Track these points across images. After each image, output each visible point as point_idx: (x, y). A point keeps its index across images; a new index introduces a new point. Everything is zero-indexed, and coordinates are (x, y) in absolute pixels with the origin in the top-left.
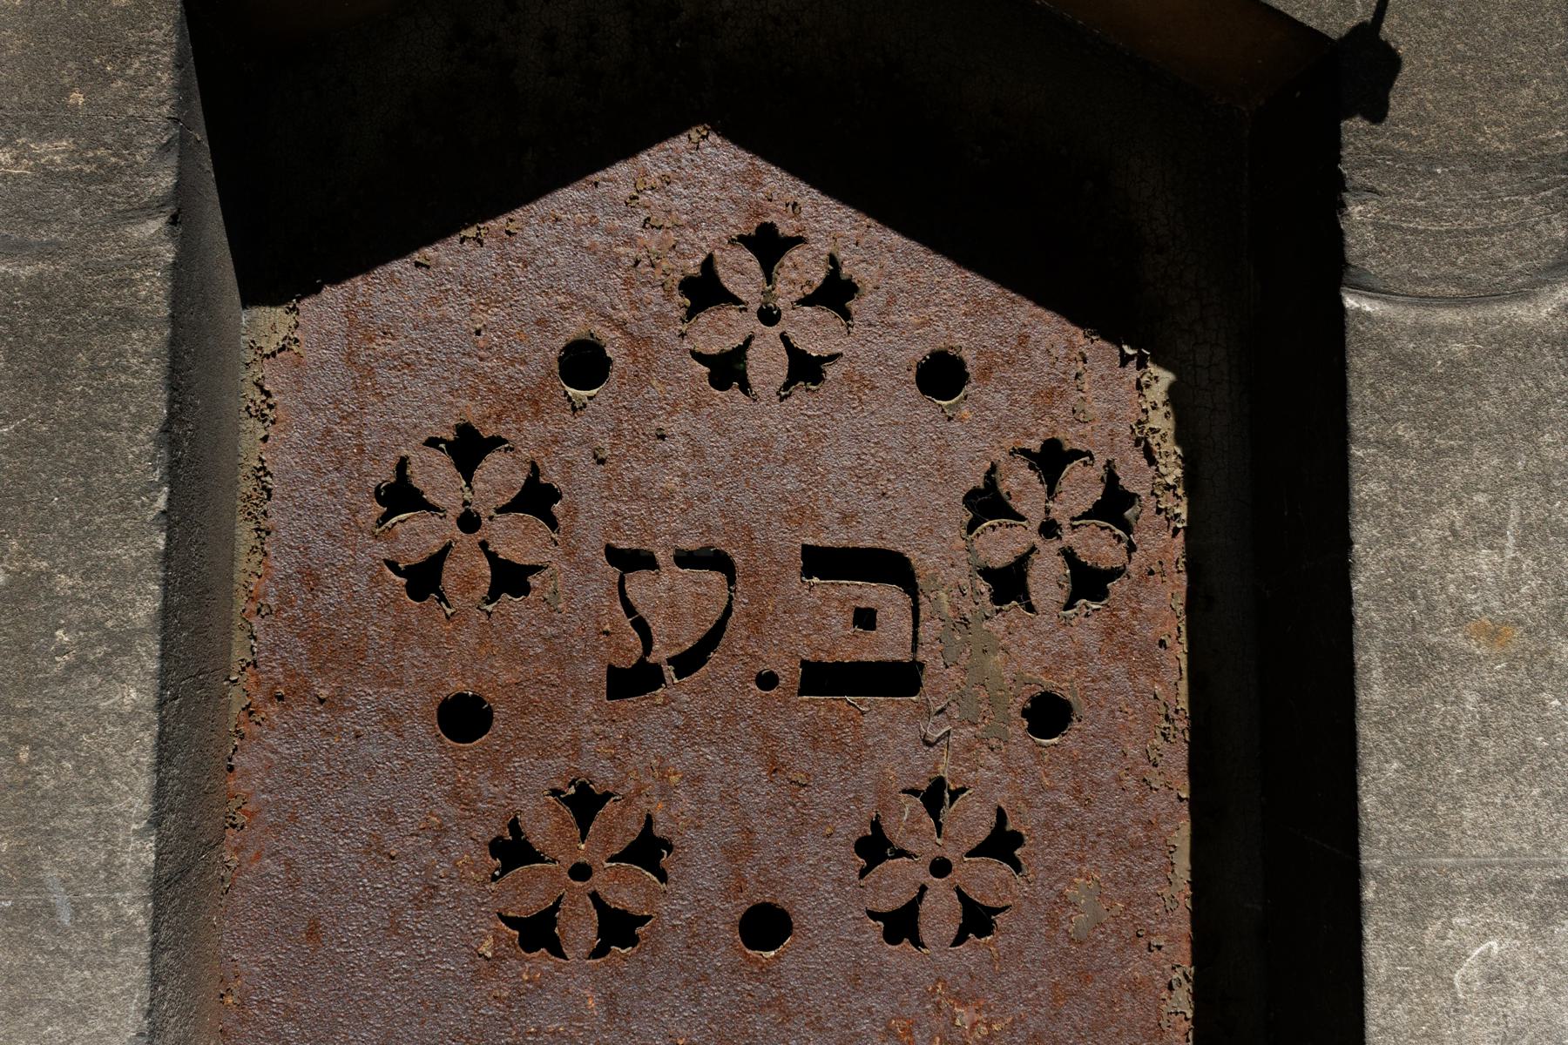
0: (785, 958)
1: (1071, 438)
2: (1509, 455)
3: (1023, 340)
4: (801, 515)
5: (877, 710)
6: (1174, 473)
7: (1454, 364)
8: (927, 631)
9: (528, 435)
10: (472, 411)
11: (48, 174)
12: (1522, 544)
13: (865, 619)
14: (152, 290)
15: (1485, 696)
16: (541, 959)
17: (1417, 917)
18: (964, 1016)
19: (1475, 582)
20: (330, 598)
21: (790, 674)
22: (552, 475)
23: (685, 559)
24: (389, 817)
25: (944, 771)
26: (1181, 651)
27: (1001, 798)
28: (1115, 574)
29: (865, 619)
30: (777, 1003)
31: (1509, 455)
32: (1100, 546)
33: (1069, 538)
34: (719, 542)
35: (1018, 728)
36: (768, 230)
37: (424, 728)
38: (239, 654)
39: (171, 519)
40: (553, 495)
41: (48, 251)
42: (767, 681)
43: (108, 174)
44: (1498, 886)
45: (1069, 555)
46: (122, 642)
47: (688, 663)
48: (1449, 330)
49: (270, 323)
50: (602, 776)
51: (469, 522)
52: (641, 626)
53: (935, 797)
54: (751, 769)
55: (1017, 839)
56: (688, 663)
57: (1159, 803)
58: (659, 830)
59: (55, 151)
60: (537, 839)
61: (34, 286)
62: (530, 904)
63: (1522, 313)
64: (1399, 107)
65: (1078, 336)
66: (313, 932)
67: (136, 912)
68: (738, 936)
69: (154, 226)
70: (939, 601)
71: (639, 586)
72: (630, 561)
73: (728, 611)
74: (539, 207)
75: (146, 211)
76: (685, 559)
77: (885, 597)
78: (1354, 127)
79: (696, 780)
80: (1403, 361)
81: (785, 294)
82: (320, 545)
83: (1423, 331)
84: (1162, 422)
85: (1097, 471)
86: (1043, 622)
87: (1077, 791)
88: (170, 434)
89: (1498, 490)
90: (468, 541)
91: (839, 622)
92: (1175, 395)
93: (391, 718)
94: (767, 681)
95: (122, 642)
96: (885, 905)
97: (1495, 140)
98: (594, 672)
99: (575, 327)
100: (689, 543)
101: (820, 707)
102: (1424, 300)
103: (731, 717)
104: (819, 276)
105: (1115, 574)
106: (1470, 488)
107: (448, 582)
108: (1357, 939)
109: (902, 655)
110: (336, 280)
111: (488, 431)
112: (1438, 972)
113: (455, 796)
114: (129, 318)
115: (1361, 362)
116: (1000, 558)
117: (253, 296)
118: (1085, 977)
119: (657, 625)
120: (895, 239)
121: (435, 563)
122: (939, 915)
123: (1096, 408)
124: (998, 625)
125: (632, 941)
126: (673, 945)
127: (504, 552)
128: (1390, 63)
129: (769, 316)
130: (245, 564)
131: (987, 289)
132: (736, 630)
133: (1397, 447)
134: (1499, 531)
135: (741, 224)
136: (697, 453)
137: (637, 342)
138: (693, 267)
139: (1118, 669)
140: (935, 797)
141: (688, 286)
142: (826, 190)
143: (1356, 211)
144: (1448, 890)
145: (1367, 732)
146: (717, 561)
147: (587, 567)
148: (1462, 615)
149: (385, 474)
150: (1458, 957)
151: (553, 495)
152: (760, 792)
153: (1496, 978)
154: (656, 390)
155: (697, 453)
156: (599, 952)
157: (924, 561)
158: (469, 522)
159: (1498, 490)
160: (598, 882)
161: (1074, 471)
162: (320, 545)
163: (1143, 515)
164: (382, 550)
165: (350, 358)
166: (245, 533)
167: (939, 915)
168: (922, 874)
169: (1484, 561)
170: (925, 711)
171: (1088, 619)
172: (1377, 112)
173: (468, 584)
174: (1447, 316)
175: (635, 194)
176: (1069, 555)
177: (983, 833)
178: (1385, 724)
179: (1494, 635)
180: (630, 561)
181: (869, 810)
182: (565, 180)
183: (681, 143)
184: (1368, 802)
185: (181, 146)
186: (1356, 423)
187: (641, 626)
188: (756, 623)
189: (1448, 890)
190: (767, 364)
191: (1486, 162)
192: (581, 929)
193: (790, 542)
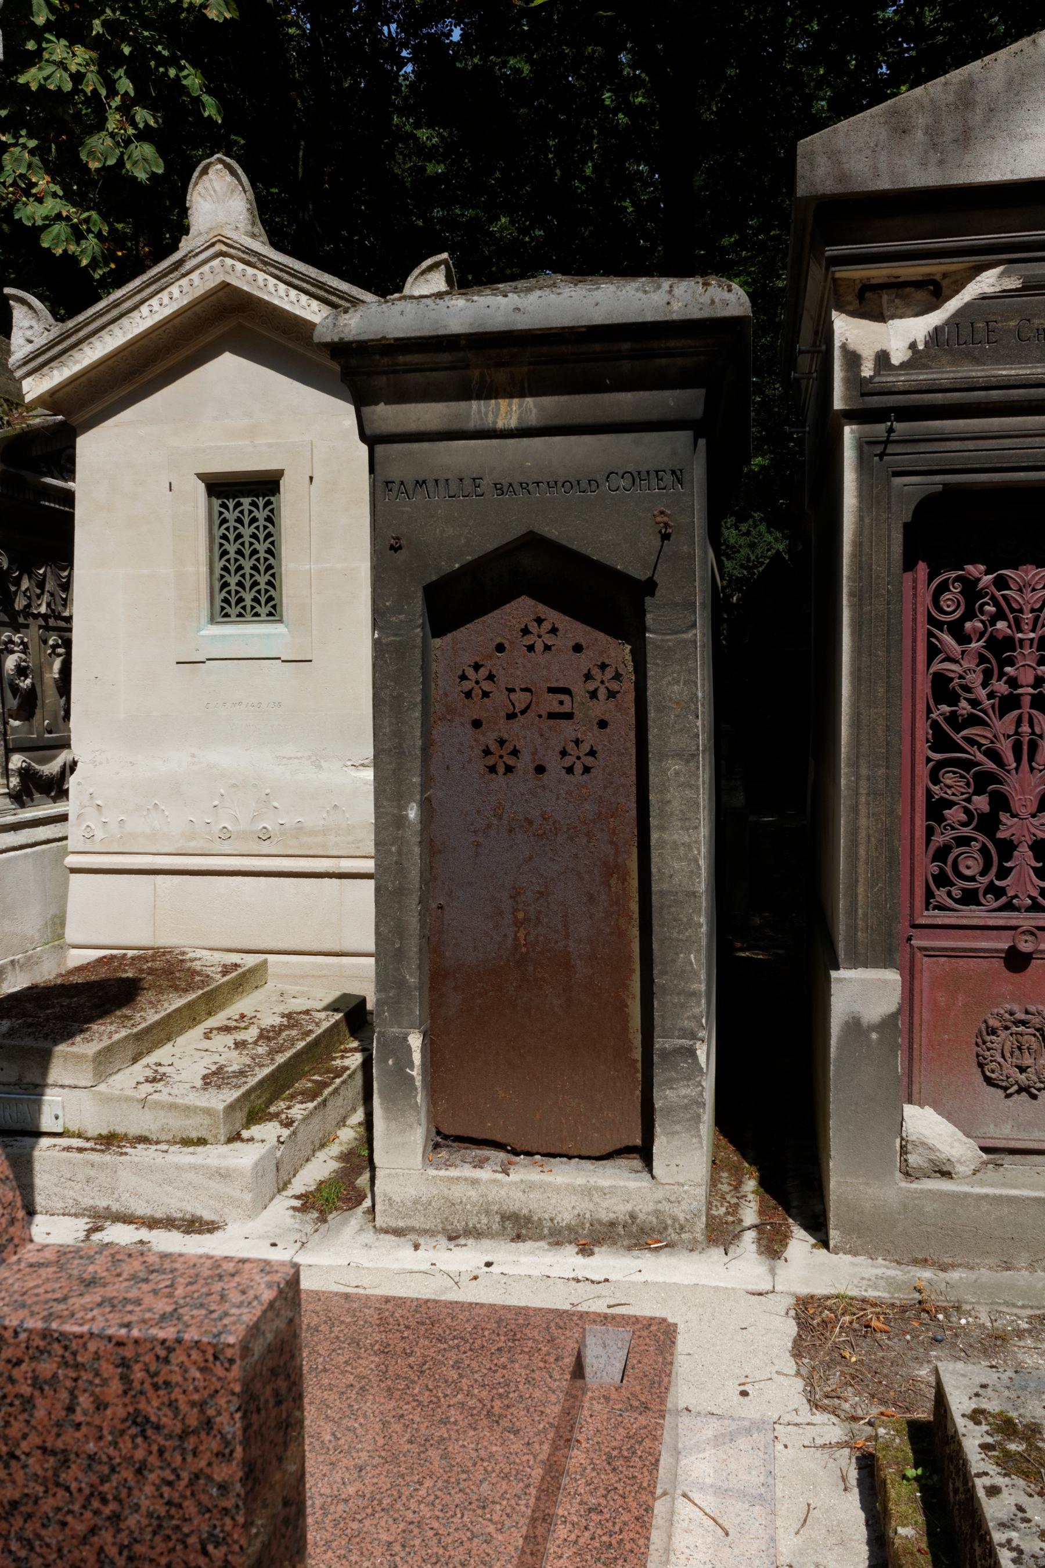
0: (545, 777)
1: (607, 662)
2: (681, 666)
3: (596, 640)
4: (547, 680)
5: (564, 723)
6: (631, 669)
7: (669, 647)
8: (575, 705)
9: (489, 664)
10: (477, 659)
11: (401, 621)
12: (684, 684)
13: (561, 703)
14: (419, 641)
15: (676, 716)
16: (494, 776)
17: (660, 761)
18: (584, 791)
19: (673, 692)
20: (450, 699)
21: (544, 714)
22: (494, 673)
23: (522, 690)
24: (462, 744)
25: (579, 736)
26: (633, 710)
27: (592, 742)
28: (618, 692)
29: (561, 703)
30: (543, 786)
31: (681, 666)
32: (614, 686)
33: (607, 684)
34: (529, 686)
35: (596, 727)
36: (539, 618)
37: (469, 726)
38: (432, 710)
39: (423, 683)
40: (494, 676)
41: (401, 635)
42: (540, 716)
43: (411, 621)
44: (677, 755)
45: (607, 688)
46: (415, 705)
47: (523, 712)
48: (668, 640)
49: (438, 642)
50: (505, 736)
51: (477, 682)
52: (513, 704)
53: (577, 742)
54: (537, 736)
55: (595, 752)
56: (523, 712)
57: (629, 744)
58: (517, 748)
59: (402, 617)
60: (492, 750)
61: (399, 642)
62: (491, 763)
63: (684, 636)
64: (658, 593)
65: (609, 638)
66: (448, 768)
67: (418, 753)
68: (994, 1510)
69: (419, 630)
70: (578, 699)
71: (513, 696)
72: (511, 690)
73: (530, 704)
74: (490, 615)
75: (417, 627)
76: (522, 690)
77: (566, 698)
78: (648, 600)
79: (525, 738)
80: (659, 647)
81: (543, 631)
82: (448, 688)
83: (663, 640)
84: (629, 657)
85: (613, 669)
86: (601, 703)
87: (609, 742)
88: (422, 668)
89: (679, 673)
90: (477, 687)
91: (555, 704)
92: (631, 651)
93: (462, 724)
94: (540, 716)
95: (415, 705)
96: (566, 766)
97: (678, 599)
98: (503, 714)
99: (499, 640)
100: (523, 686)
101: (551, 722)
102: (663, 634)
103: (532, 724)
104: (550, 627)
105: (618, 692)
106: (673, 673)
107: (473, 695)
108: (648, 765)
109: (569, 711)
110: (450, 632)
111: (481, 663)
112: (665, 772)
113: (475, 740)
114: (415, 647)
115: (649, 647)
116: (591, 689)
117: (434, 636)
118: (612, 783)
119: (516, 704)
120: (567, 618)
121: (471, 691)
122: (578, 768)
123: (613, 655)
124: (591, 704)
125: (512, 772)
126: (521, 773)
127: (485, 689)
128: (656, 585)
129: (539, 636)
130: (433, 692)
131: (588, 628)
132: (533, 706)
133: (657, 665)
134: (679, 682)
135: (533, 617)
136: (524, 667)
137: (511, 643)
138: (523, 627)
139: (619, 714)
140: (577, 742)
141: (522, 630)
142: (552, 608)
143: (648, 616)
144: (667, 756)
145: (650, 723)
146: (526, 690)
147: (501, 692)
148: (671, 699)
149: (460, 673)
150: (669, 769)
151: (494, 676)
152: (539, 740)
153: (677, 773)
154: (516, 653)
155: (524, 667)
156: (505, 774)
157: (574, 690)
158: (477, 682)
159: (679, 673)
160: (505, 759)
161: (608, 669)
162: (448, 688)
163: (625, 678)
164: (460, 689)
165: (453, 649)
166: (433, 685)
167: (578, 768)
168: (574, 759)
169: (676, 688)
170: (574, 723)
171: (611, 704)
172: (653, 595)
173: (477, 696)
174: (668, 637)
175: (110, 1497)
176: (607, 688)
177: (588, 750)
178: (654, 721)
179: (678, 703)
180: (511, 690)
181: (562, 744)
182: (496, 609)
183: (520, 599)
184: (650, 737)
185: (422, 615)
186: (648, 660)
187: (513, 704)
188: (537, 704)
189: (667, 756)
190: (539, 647)
191: (677, 605)
192: (501, 769)
193: (545, 686)
